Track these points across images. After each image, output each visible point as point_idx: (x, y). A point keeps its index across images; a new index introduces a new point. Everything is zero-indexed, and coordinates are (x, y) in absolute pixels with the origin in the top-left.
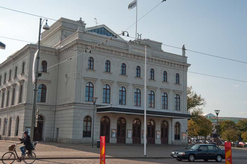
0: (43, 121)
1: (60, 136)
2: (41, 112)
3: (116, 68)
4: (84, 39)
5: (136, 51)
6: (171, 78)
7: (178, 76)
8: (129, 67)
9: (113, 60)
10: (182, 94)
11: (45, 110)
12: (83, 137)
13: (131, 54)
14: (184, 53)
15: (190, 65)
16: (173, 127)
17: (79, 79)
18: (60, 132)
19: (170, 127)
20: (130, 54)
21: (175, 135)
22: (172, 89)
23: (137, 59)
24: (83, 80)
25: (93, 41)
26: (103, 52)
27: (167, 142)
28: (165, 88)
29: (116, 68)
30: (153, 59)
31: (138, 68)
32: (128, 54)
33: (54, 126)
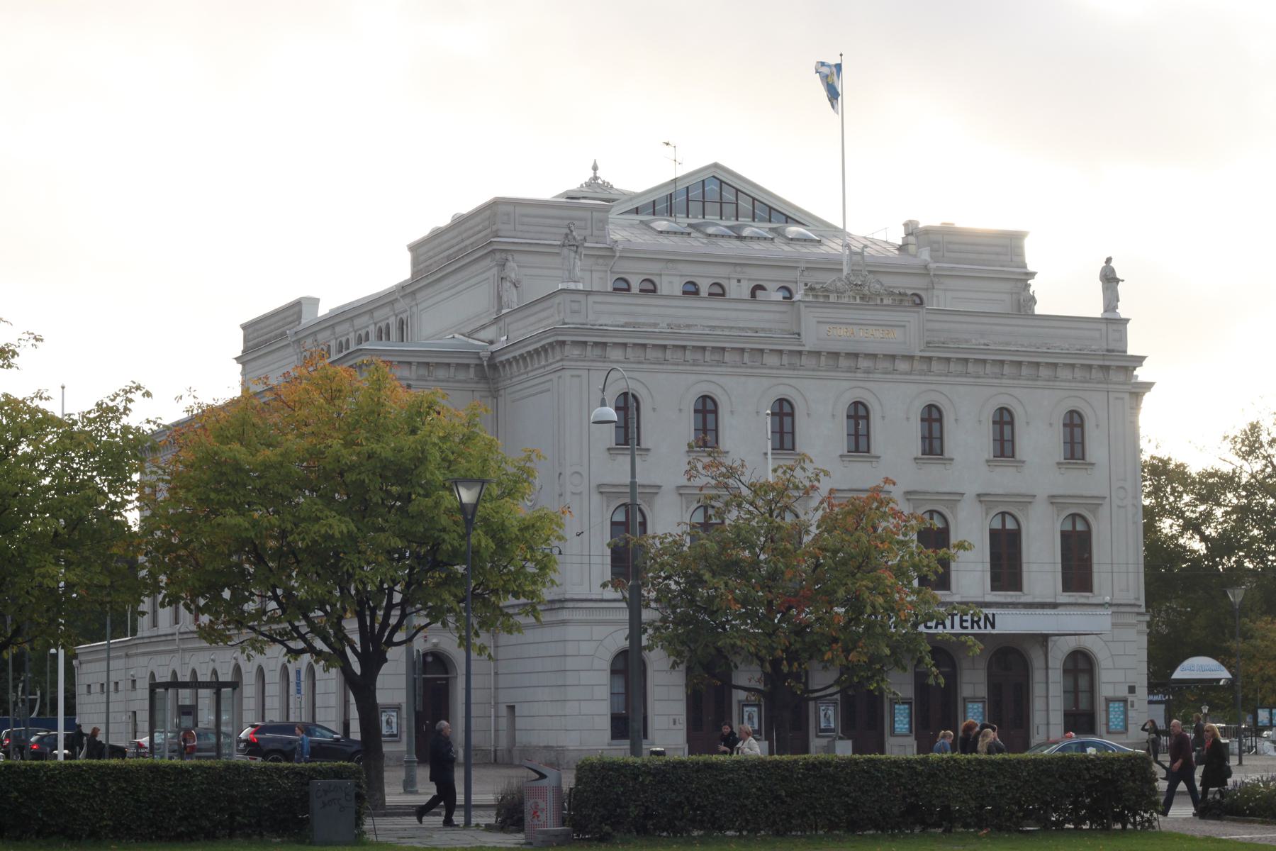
0: (447, 679)
1: (521, 738)
3: (968, 437)
6: (1039, 439)
7: (1074, 424)
10: (1104, 511)
12: (614, 737)
13: (818, 353)
14: (1111, 300)
15: (1143, 358)
16: (1056, 675)
17: (1124, 507)
18: (520, 723)
19: (1038, 676)
20: (809, 352)
21: (1065, 715)
23: (849, 370)
24: (596, 498)
28: (1001, 492)
29: (968, 437)
30: (930, 359)
31: (704, 404)
32: (800, 353)
33: (496, 697)
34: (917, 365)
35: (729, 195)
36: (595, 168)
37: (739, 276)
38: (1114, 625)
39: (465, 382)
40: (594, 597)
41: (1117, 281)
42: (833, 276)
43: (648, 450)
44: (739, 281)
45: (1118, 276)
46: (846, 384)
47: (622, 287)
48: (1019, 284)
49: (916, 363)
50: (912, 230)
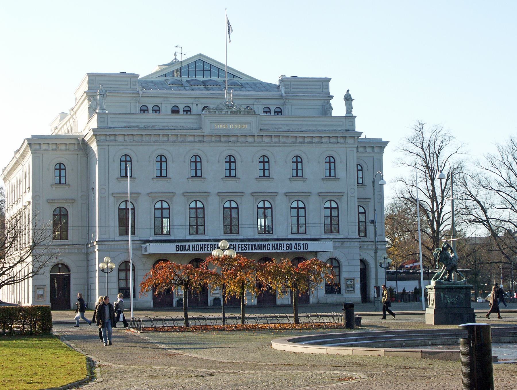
2: (61, 259)
4: (110, 125)
5: (222, 126)
8: (173, 161)
9: (169, 150)
10: (344, 198)
11: (70, 254)
14: (349, 109)
22: (282, 190)
23: (225, 142)
24: (112, 199)
25: (128, 125)
26: (209, 143)
27: (309, 301)
34: (256, 139)
35: (207, 67)
36: (175, 55)
37: (197, 103)
38: (334, 247)
39: (73, 151)
40: (111, 240)
41: (352, 100)
42: (219, 101)
43: (273, 178)
44: (197, 105)
45: (353, 98)
46: (188, 148)
47: (144, 110)
48: (326, 101)
49: (256, 138)
50: (102, 88)
